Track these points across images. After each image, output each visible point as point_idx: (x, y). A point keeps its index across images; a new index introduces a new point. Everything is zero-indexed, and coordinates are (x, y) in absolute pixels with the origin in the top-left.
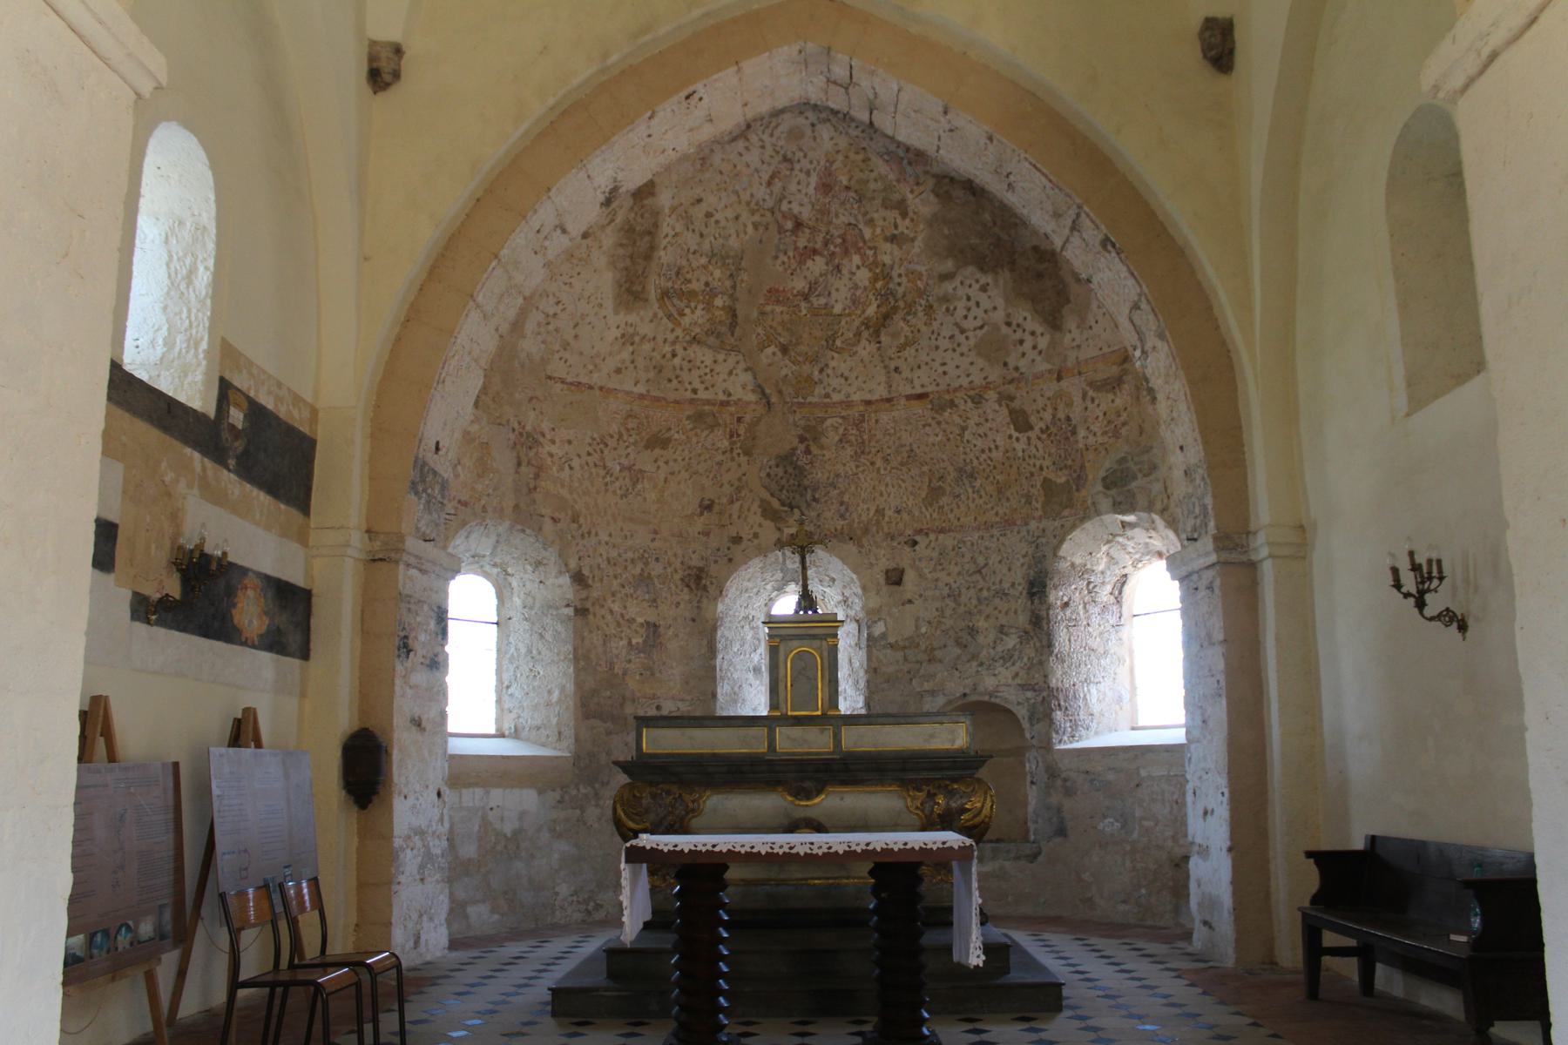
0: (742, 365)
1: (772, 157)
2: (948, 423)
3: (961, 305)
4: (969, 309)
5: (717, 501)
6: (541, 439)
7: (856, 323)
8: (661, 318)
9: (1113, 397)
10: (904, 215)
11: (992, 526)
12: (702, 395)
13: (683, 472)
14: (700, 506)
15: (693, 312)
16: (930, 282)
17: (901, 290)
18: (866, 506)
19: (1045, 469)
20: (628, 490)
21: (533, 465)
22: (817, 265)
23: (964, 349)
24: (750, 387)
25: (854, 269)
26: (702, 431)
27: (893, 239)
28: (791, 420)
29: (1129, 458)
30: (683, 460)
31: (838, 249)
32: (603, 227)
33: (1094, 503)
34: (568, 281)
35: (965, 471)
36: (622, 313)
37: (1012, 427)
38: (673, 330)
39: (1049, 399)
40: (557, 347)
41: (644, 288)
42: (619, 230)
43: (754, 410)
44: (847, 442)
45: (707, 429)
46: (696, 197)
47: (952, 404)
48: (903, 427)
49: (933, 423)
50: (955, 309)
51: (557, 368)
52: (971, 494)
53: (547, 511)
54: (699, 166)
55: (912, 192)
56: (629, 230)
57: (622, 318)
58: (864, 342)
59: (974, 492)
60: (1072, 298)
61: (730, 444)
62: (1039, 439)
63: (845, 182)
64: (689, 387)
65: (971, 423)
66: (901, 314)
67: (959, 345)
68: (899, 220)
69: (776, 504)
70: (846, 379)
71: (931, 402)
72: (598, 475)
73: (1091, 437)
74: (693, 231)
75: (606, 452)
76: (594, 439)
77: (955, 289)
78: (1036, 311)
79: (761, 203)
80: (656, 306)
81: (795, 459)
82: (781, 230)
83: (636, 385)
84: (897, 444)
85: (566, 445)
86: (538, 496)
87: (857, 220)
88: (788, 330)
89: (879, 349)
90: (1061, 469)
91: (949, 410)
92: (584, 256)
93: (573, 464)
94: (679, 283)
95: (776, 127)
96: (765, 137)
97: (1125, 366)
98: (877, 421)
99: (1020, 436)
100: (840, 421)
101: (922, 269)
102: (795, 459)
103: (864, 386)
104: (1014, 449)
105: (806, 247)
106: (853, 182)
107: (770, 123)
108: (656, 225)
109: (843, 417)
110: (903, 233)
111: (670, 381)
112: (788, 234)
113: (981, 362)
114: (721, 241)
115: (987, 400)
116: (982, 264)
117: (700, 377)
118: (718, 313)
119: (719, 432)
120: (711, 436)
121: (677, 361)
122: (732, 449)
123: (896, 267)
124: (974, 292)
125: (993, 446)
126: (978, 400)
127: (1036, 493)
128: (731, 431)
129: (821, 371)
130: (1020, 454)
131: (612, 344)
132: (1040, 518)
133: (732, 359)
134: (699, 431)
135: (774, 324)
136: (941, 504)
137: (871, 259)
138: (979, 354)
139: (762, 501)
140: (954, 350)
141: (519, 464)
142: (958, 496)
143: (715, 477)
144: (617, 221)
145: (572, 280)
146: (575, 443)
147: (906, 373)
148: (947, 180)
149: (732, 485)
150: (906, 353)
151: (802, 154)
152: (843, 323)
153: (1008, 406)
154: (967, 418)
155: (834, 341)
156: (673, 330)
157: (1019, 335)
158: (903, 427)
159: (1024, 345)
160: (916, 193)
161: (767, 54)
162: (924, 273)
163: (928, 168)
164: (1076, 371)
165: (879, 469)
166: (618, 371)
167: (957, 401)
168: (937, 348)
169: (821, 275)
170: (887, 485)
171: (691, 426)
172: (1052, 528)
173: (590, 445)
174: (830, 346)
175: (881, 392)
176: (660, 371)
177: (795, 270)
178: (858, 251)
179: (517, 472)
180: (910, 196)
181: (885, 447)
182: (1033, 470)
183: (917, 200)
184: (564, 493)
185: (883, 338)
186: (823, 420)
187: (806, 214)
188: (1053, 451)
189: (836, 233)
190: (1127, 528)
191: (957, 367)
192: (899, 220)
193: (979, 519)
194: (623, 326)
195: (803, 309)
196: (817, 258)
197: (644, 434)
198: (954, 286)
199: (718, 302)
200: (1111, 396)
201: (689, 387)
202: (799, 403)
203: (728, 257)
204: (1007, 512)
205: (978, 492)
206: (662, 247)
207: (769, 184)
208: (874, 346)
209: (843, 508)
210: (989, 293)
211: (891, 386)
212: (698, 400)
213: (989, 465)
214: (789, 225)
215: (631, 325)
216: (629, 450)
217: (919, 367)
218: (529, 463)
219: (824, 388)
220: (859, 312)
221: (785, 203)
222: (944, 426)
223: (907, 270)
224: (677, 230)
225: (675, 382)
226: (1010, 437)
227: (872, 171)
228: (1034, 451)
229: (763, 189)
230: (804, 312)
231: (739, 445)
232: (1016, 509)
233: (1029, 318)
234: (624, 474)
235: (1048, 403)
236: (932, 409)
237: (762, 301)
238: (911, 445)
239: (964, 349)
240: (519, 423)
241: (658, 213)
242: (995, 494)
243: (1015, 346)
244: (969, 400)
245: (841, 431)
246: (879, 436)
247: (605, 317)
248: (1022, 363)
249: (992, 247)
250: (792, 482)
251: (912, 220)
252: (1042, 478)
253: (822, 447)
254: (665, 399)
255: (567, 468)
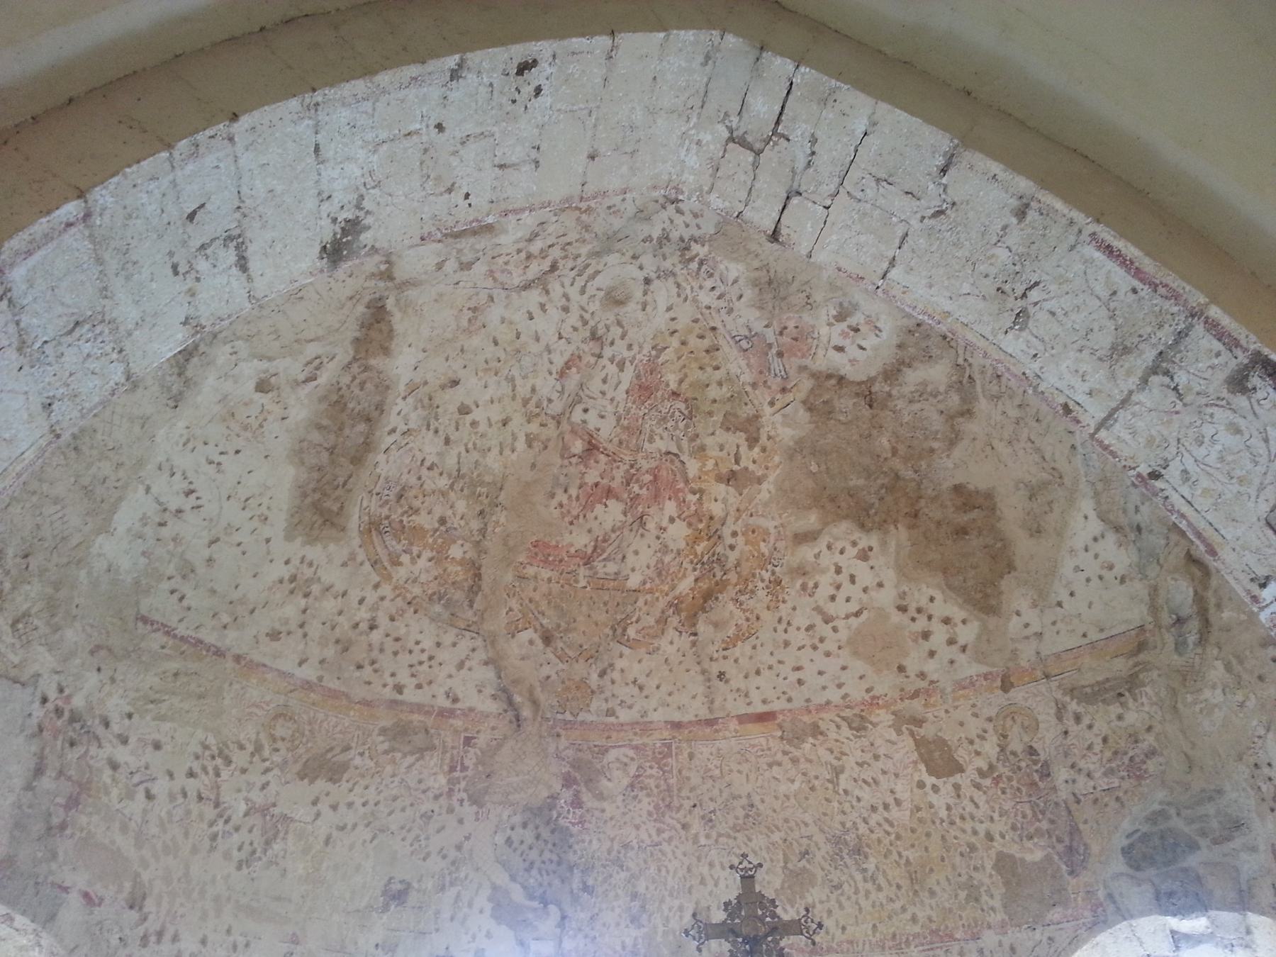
0: (481, 655)
1: (575, 329)
2: (810, 761)
3: (826, 582)
4: (838, 587)
5: (415, 885)
6: (100, 730)
7: (662, 604)
8: (361, 564)
9: (1120, 710)
10: (753, 441)
11: (908, 943)
12: (410, 695)
13: (360, 827)
14: (385, 893)
15: (413, 561)
16: (780, 545)
17: (733, 557)
18: (676, 903)
19: (997, 837)
20: (254, 852)
21: (69, 778)
22: (612, 513)
23: (830, 645)
24: (489, 691)
25: (665, 523)
26: (405, 756)
27: (730, 478)
28: (552, 749)
29: (1172, 811)
30: (364, 805)
31: (644, 492)
32: (297, 384)
33: (1110, 896)
34: (217, 458)
35: (846, 843)
36: (299, 540)
37: (922, 767)
38: (376, 586)
39: (990, 720)
40: (171, 570)
41: (342, 508)
42: (323, 399)
43: (493, 729)
44: (642, 789)
45: (412, 753)
46: (451, 375)
47: (816, 731)
48: (735, 767)
49: (786, 760)
50: (816, 586)
51: (159, 604)
52: (861, 885)
53: (79, 880)
54: (465, 323)
55: (772, 404)
56: (336, 403)
57: (296, 549)
58: (671, 633)
59: (865, 880)
60: (1018, 563)
61: (449, 781)
62: (978, 786)
63: (673, 386)
64: (390, 681)
65: (849, 762)
66: (731, 591)
67: (822, 640)
68: (743, 449)
69: (517, 894)
70: (641, 688)
71: (780, 727)
72: (201, 817)
73: (1082, 779)
74: (436, 432)
75: (225, 774)
76: (206, 747)
77: (817, 556)
78: (950, 587)
79: (545, 404)
80: (356, 541)
81: (555, 814)
82: (565, 452)
83: (300, 664)
84: (725, 795)
85: (150, 749)
86: (64, 846)
87: (679, 448)
88: (557, 607)
89: (694, 644)
90: (1030, 838)
91: (811, 740)
92: (255, 425)
93: (155, 790)
94: (400, 511)
95: (593, 277)
96: (573, 292)
97: (1142, 657)
98: (691, 756)
99: (940, 782)
100: (631, 753)
101: (770, 524)
102: (555, 814)
103: (669, 699)
104: (931, 806)
105: (597, 485)
106: (685, 386)
107: (587, 266)
108: (380, 408)
109: (636, 748)
110: (746, 469)
111: (360, 667)
112: (574, 460)
113: (859, 666)
114: (475, 455)
115: (875, 725)
116: (863, 517)
117: (411, 666)
118: (453, 568)
119: (432, 760)
120: (418, 765)
121: (376, 636)
122: (451, 790)
123: (730, 520)
124: (849, 561)
125: (890, 800)
126: (859, 725)
127: (987, 881)
128: (452, 759)
129: (602, 674)
130: (943, 813)
131: (270, 589)
132: (1003, 925)
133: (465, 644)
134: (398, 755)
135: (537, 597)
136: (810, 900)
137: (693, 508)
138: (856, 653)
139: (495, 888)
140: (815, 648)
141: (39, 771)
142: (838, 887)
143: (417, 838)
144: (319, 381)
145: (222, 458)
146: (168, 748)
147: (737, 681)
148: (833, 382)
149: (444, 857)
150: (736, 652)
151: (620, 331)
152: (640, 603)
153: (912, 734)
154: (843, 754)
155: (625, 630)
156: (376, 586)
157: (922, 624)
158: (735, 767)
159: (932, 638)
160: (778, 405)
161: (662, 35)
162: (772, 531)
163: (807, 362)
164: (1039, 674)
165: (696, 839)
166: (274, 635)
167: (823, 725)
168: (786, 644)
169: (613, 531)
170: (711, 865)
171: (386, 746)
172: (1030, 944)
173: (197, 757)
174: (618, 631)
175: (697, 709)
176: (346, 649)
177: (577, 517)
178: (675, 495)
179: (29, 787)
180: (768, 410)
181: (706, 798)
182: (973, 839)
183: (778, 417)
184: (124, 843)
185: (701, 627)
186: (603, 751)
187: (606, 430)
188: (1008, 806)
189: (645, 465)
190: (1183, 944)
191: (820, 673)
192: (743, 449)
193: (881, 927)
194: (296, 561)
195: (581, 578)
196: (612, 503)
197: (301, 750)
198: (816, 550)
199: (456, 552)
200: (1115, 709)
201: (390, 681)
202: (566, 722)
203: (482, 484)
204: (934, 915)
205: (873, 879)
206: (384, 447)
207: (562, 374)
208: (686, 640)
209: (637, 904)
210: (871, 563)
211: (712, 702)
212: (402, 703)
213: (888, 833)
214: (578, 446)
215: (311, 564)
216: (269, 776)
217: (758, 673)
218: (61, 773)
219: (606, 700)
220: (666, 588)
221: (578, 409)
222: (803, 765)
223: (747, 525)
224: (412, 425)
225: (368, 669)
226: (921, 785)
227: (717, 368)
228: (970, 808)
229: (551, 381)
230: (583, 583)
231: (463, 784)
232: (950, 910)
233: (939, 596)
234: (250, 821)
235: (989, 727)
236: (782, 738)
237: (522, 558)
238: (749, 796)
239: (830, 645)
240: (61, 690)
241: (388, 387)
242: (905, 883)
243: (915, 641)
244: (844, 725)
245: (632, 770)
246: (695, 780)
247: (268, 541)
248: (931, 667)
249: (883, 491)
250: (547, 855)
251: (764, 450)
252: (993, 853)
253: (601, 797)
254: (347, 696)
255: (141, 795)
